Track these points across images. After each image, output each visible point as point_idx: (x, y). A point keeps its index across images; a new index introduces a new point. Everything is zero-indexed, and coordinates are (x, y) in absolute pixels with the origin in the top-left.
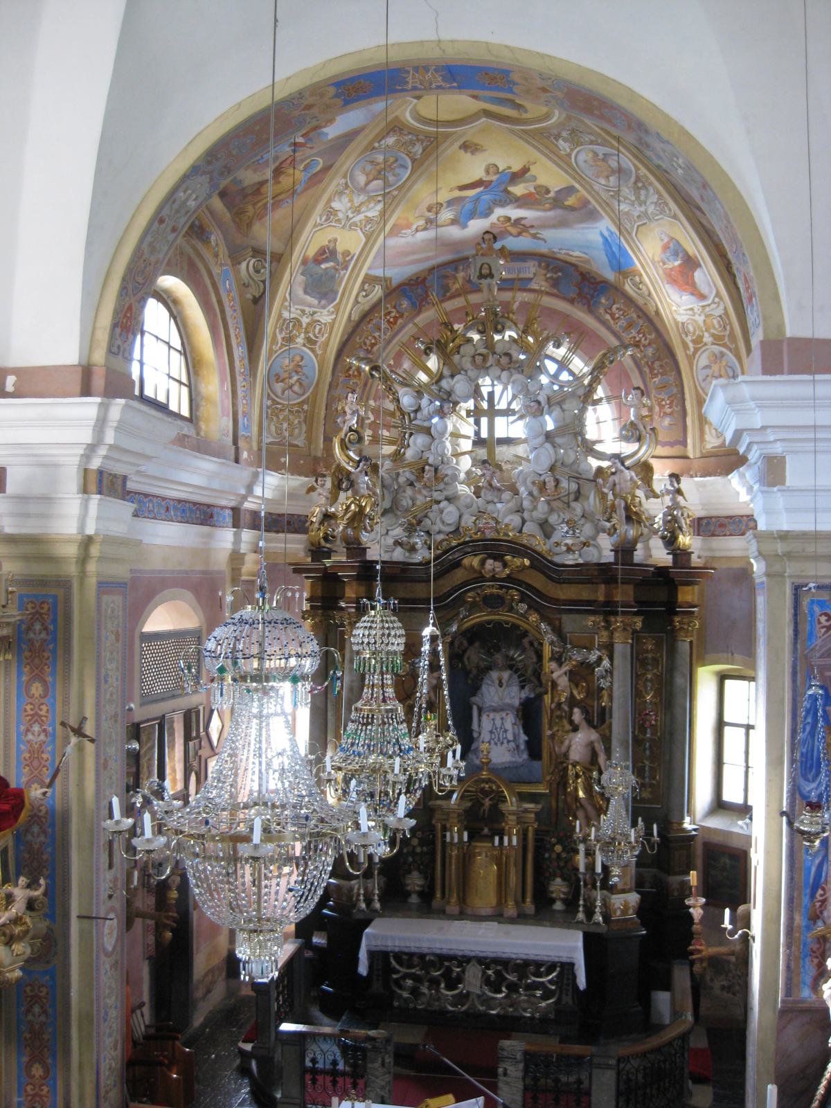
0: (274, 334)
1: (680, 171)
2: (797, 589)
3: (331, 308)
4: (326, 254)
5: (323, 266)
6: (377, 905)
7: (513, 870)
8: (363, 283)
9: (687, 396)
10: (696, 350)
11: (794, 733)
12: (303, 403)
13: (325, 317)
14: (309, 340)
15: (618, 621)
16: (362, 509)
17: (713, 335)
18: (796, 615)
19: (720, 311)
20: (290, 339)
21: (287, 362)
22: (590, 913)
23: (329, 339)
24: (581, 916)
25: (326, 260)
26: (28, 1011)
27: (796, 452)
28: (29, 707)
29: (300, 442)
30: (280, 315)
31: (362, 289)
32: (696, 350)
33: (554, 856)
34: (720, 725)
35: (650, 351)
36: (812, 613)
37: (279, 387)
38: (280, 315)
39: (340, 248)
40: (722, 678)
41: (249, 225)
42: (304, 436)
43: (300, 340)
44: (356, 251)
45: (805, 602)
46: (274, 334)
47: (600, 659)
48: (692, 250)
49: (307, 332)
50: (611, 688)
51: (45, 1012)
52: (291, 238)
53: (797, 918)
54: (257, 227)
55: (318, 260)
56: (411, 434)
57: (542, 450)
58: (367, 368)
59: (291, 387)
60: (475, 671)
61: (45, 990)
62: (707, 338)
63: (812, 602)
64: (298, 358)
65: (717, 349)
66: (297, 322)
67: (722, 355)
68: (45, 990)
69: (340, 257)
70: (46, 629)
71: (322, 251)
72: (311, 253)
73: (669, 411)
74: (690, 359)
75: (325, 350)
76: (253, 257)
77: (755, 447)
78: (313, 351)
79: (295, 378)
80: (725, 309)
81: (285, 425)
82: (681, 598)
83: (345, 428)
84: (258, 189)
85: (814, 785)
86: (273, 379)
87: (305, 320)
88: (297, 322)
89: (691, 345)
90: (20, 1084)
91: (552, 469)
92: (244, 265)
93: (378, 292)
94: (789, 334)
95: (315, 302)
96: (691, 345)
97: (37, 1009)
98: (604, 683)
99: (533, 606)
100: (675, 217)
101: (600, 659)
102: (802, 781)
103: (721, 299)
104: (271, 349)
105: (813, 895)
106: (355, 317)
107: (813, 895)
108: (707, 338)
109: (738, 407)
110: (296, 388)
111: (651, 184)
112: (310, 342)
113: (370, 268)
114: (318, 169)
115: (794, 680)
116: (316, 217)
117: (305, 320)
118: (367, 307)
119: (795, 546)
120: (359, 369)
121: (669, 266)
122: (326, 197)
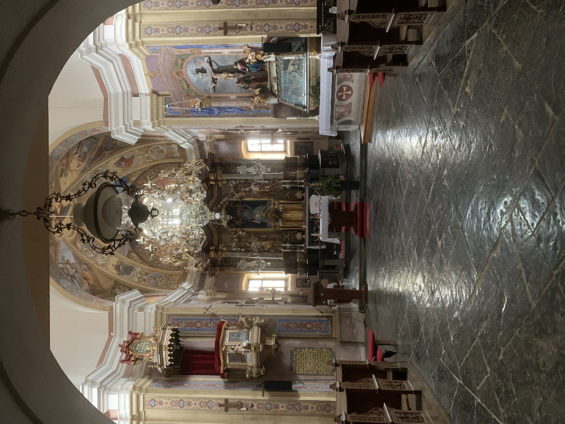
0: (142, 285)
1: (64, 149)
2: (166, 117)
3: (136, 268)
4: (117, 268)
5: (121, 269)
6: (303, 245)
7: (294, 207)
8: (129, 258)
9: (164, 162)
10: (151, 159)
11: (202, 117)
12: (166, 277)
13: (139, 270)
14: (145, 275)
15: (219, 178)
16: (187, 252)
17: (145, 153)
18: (173, 117)
19: (137, 151)
20: (145, 280)
21: (152, 281)
22: (302, 184)
23: (146, 269)
24: (303, 186)
25: (119, 268)
26: (291, 328)
27: (132, 117)
28: (204, 327)
29: (178, 278)
30: (136, 283)
31: (131, 259)
32: (151, 159)
33: (289, 196)
34: (262, 152)
35: (153, 173)
36: (172, 112)
37: (159, 284)
38: (136, 283)
39: (116, 264)
40: (248, 151)
41: (103, 289)
42: (176, 277)
43: (145, 277)
44: (117, 259)
45: (170, 114)
46: (142, 285)
47: (232, 183)
48: (118, 159)
49: (143, 275)
50: (240, 180)
51: (291, 323)
52: (109, 278)
53: (251, 114)
54: (105, 288)
55: (119, 270)
56: (173, 242)
57: (178, 203)
58: (152, 255)
59: (160, 280)
60: (243, 222)
61: (285, 323)
62: (147, 155)
63: (170, 112)
64: (151, 278)
65: (150, 152)
66: (139, 278)
67: (151, 151)
68: (285, 323)
69: (119, 264)
70: (182, 322)
71: (116, 269)
72: (116, 272)
73: (170, 168)
74: (154, 161)
75: (150, 270)
76: (115, 289)
77: (132, 128)
78: (149, 274)
79: (158, 279)
80: (137, 149)
81: (172, 282)
82: (218, 162)
83: (170, 261)
84: (91, 285)
85: (216, 111)
86: (157, 285)
87: (139, 275)
88: (139, 278)
89: (149, 160)
90: (313, 332)
91: (183, 200)
92: (117, 292)
93: (133, 254)
94: (102, 119)
95: (133, 272)
96: (149, 160)
97: (290, 326)
98: (238, 182)
99: (219, 203)
100: (107, 163)
101: (232, 183)
102: (215, 115)
103: (133, 151)
104: (147, 286)
105: (244, 110)
106: (141, 261)
107: (244, 110)
108: (147, 155)
109: (119, 132)
110: (161, 279)
111: (96, 169)
112: (146, 274)
113: (124, 256)
114: (86, 267)
115: (190, 117)
116: (104, 270)
117: (139, 275)
118: (138, 258)
119: (155, 117)
120: (152, 257)
121: (124, 165)
122: (98, 267)
